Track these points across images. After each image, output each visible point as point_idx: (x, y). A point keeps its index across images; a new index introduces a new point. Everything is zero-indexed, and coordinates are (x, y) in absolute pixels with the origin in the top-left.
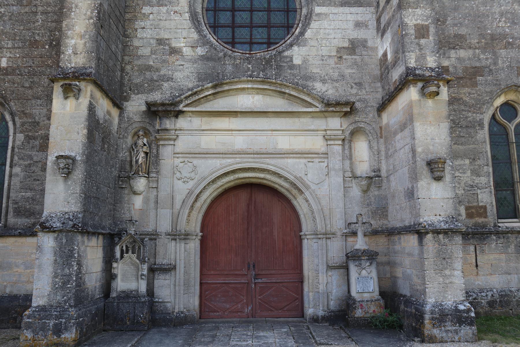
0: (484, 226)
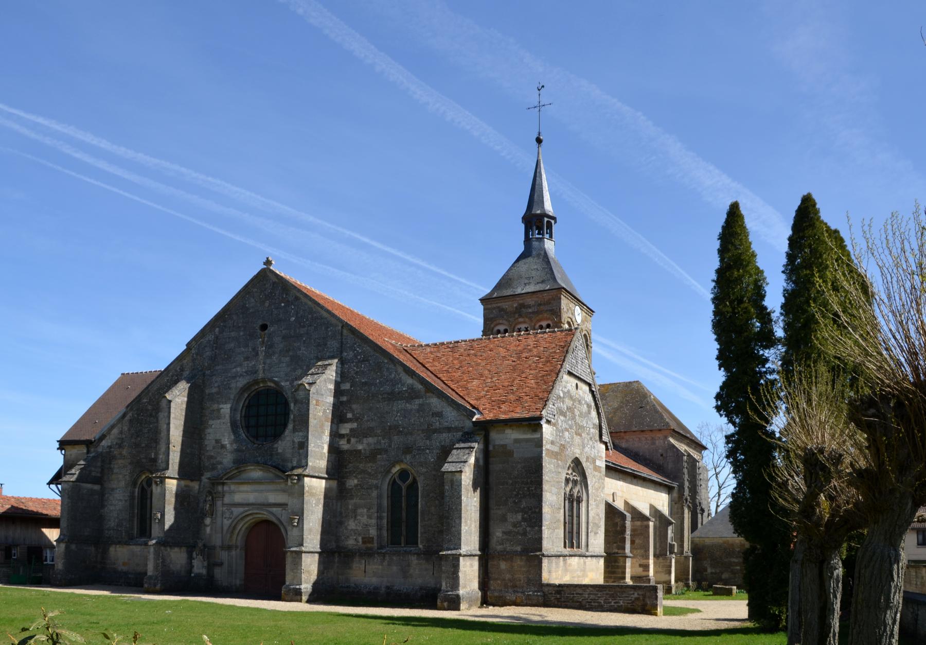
0: (371, 549)
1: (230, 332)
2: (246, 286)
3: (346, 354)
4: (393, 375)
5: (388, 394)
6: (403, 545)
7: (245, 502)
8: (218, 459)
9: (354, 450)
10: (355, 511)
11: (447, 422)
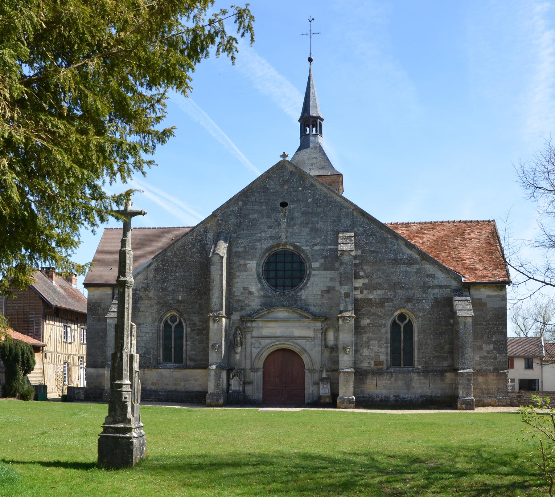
0: (382, 369)
1: (253, 205)
2: (268, 172)
3: (356, 229)
4: (396, 247)
5: (392, 260)
6: (402, 366)
7: (272, 335)
8: (246, 302)
9: (367, 299)
10: (368, 342)
11: (438, 281)
